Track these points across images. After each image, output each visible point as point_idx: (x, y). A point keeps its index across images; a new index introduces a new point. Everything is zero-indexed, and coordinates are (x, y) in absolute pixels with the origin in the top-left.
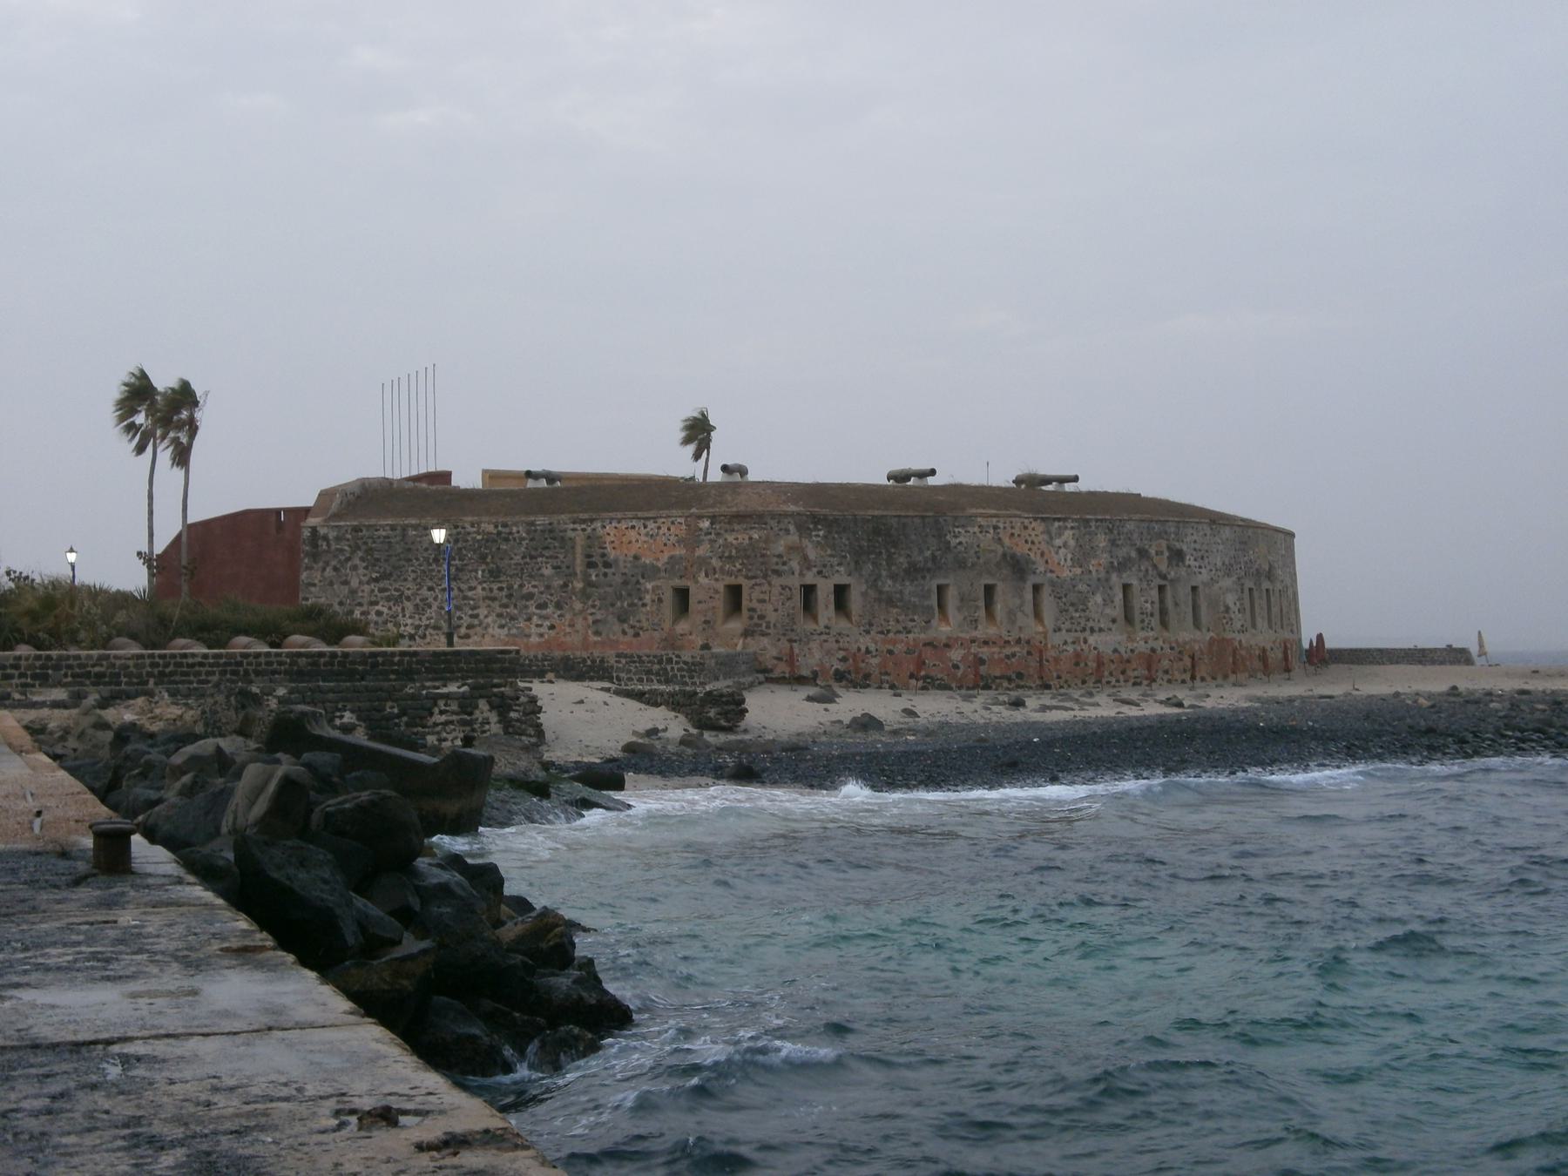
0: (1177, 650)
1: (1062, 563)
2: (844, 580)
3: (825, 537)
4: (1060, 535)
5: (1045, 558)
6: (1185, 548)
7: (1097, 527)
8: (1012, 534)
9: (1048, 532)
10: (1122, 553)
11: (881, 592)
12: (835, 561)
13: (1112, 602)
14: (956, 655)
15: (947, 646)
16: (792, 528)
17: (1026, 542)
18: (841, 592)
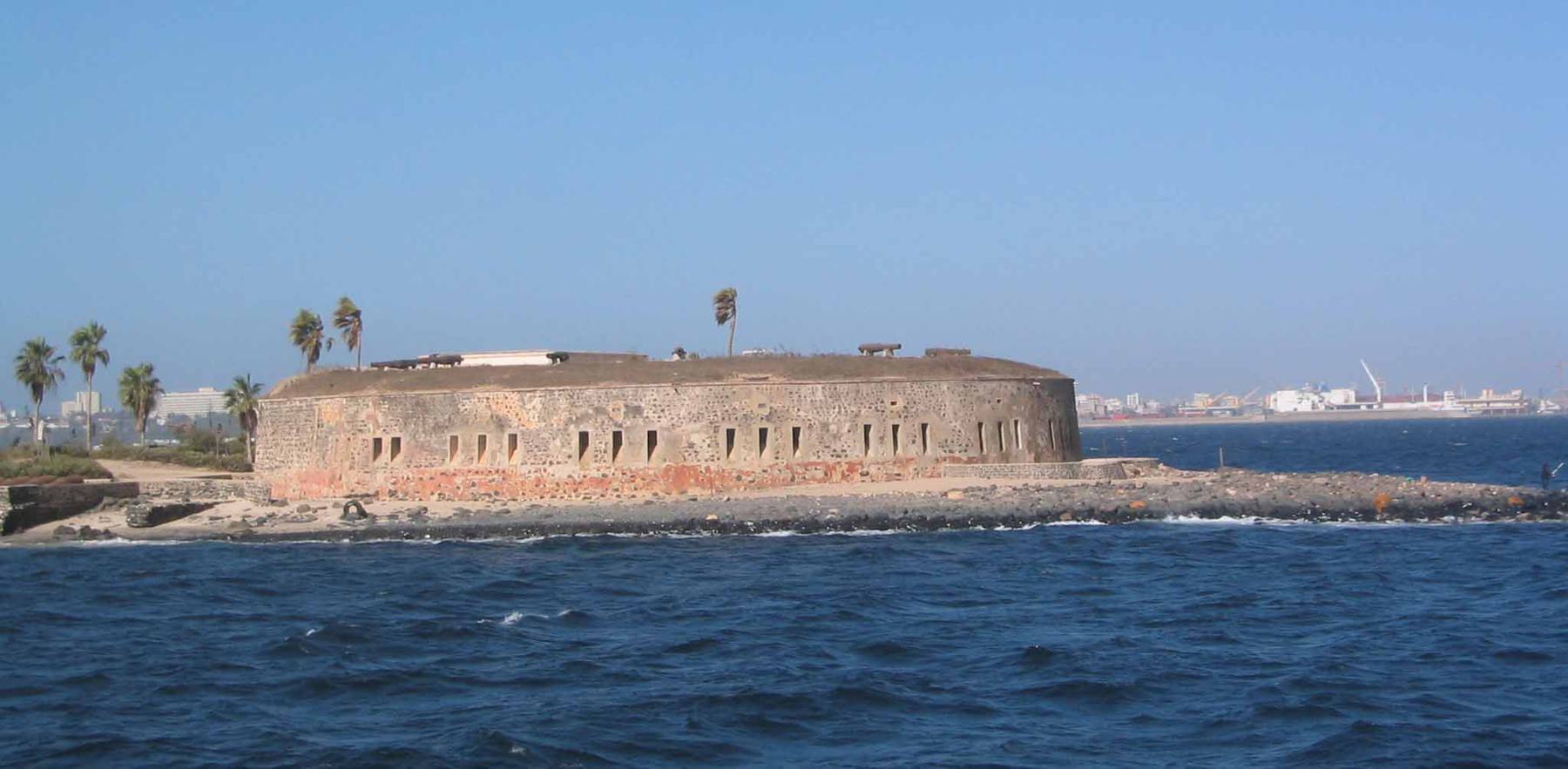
0: (629, 474)
1: (531, 419)
2: (397, 435)
3: (389, 409)
4: (531, 401)
5: (519, 416)
6: (643, 405)
7: (560, 395)
8: (498, 403)
9: (523, 400)
10: (579, 412)
11: (417, 442)
12: (393, 423)
13: (569, 444)
14: (458, 480)
15: (454, 475)
16: (370, 404)
17: (506, 407)
18: (396, 442)
